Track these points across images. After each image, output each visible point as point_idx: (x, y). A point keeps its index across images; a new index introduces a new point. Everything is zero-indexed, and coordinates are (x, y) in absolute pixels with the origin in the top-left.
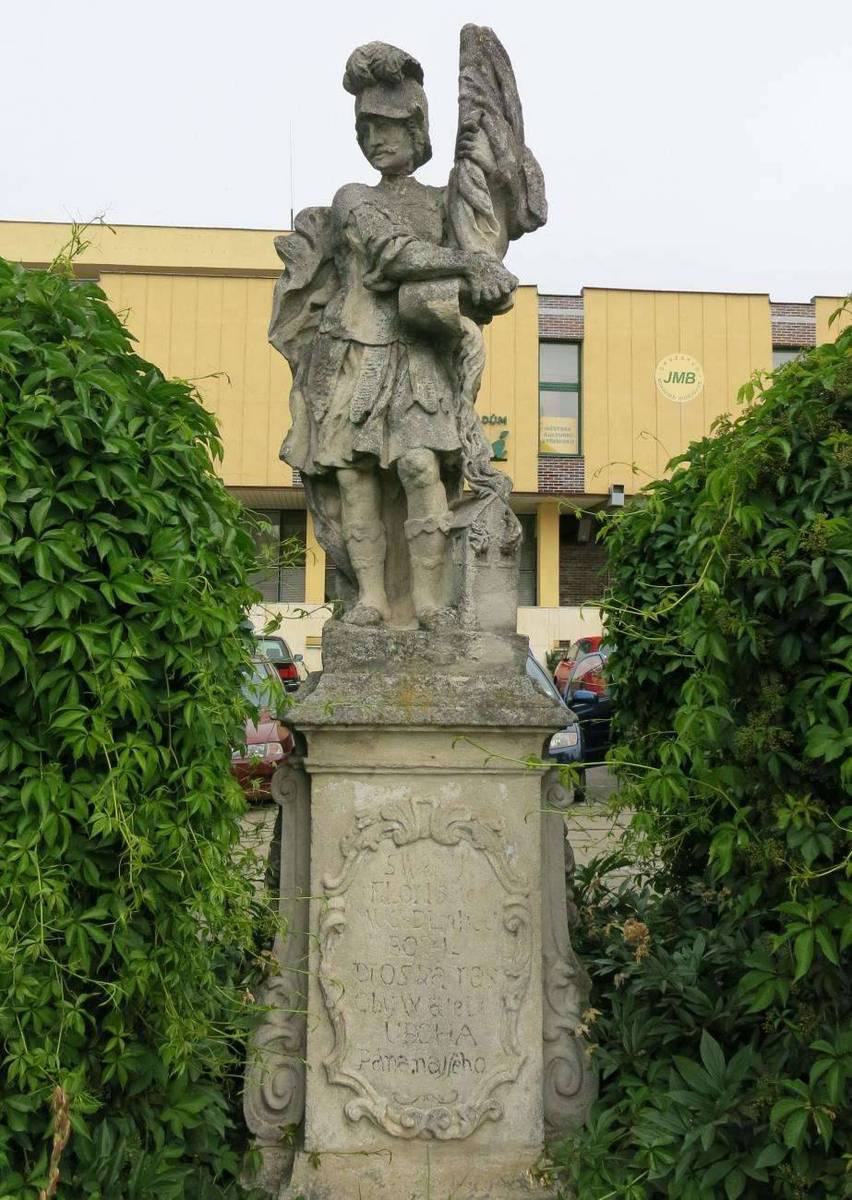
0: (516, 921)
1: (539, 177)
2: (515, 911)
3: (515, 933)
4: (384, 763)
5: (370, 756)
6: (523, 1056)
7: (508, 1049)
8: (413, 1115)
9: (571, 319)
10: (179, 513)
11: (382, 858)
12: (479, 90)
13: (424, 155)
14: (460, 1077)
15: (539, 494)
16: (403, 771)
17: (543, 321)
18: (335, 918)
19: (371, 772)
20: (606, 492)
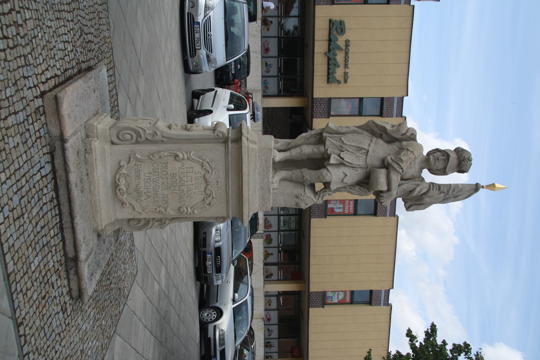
1: (424, 209)
2: (186, 210)
3: (179, 210)
6: (143, 213)
7: (144, 208)
9: (392, 112)
12: (454, 190)
13: (432, 171)
15: (313, 98)
17: (391, 99)
20: (313, 128)
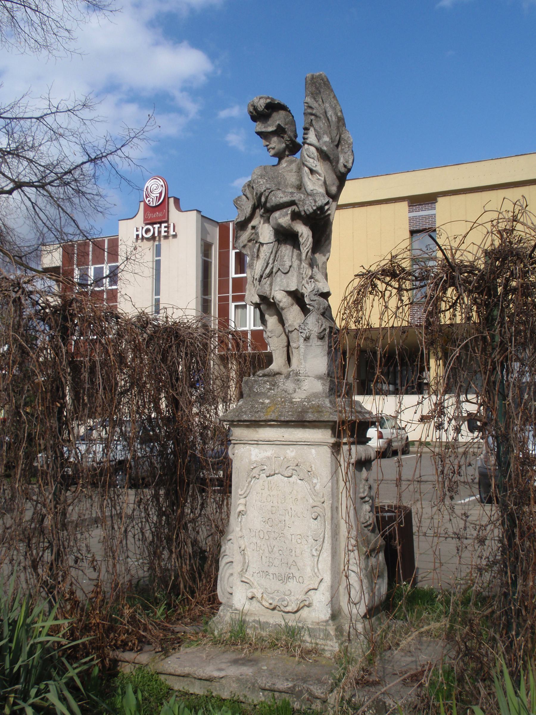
0: (316, 514)
4: (261, 439)
5: (257, 436)
6: (320, 578)
8: (272, 598)
10: (493, 349)
11: (261, 481)
14: (292, 585)
16: (270, 442)
18: (241, 508)
19: (257, 443)
